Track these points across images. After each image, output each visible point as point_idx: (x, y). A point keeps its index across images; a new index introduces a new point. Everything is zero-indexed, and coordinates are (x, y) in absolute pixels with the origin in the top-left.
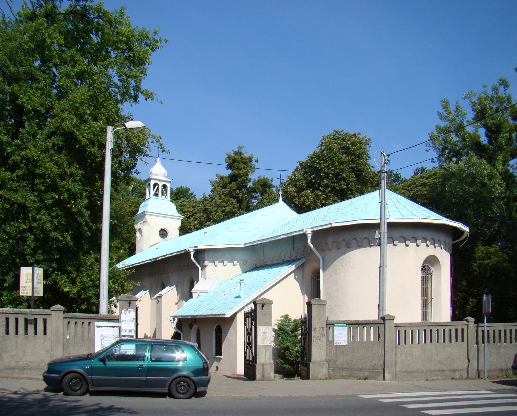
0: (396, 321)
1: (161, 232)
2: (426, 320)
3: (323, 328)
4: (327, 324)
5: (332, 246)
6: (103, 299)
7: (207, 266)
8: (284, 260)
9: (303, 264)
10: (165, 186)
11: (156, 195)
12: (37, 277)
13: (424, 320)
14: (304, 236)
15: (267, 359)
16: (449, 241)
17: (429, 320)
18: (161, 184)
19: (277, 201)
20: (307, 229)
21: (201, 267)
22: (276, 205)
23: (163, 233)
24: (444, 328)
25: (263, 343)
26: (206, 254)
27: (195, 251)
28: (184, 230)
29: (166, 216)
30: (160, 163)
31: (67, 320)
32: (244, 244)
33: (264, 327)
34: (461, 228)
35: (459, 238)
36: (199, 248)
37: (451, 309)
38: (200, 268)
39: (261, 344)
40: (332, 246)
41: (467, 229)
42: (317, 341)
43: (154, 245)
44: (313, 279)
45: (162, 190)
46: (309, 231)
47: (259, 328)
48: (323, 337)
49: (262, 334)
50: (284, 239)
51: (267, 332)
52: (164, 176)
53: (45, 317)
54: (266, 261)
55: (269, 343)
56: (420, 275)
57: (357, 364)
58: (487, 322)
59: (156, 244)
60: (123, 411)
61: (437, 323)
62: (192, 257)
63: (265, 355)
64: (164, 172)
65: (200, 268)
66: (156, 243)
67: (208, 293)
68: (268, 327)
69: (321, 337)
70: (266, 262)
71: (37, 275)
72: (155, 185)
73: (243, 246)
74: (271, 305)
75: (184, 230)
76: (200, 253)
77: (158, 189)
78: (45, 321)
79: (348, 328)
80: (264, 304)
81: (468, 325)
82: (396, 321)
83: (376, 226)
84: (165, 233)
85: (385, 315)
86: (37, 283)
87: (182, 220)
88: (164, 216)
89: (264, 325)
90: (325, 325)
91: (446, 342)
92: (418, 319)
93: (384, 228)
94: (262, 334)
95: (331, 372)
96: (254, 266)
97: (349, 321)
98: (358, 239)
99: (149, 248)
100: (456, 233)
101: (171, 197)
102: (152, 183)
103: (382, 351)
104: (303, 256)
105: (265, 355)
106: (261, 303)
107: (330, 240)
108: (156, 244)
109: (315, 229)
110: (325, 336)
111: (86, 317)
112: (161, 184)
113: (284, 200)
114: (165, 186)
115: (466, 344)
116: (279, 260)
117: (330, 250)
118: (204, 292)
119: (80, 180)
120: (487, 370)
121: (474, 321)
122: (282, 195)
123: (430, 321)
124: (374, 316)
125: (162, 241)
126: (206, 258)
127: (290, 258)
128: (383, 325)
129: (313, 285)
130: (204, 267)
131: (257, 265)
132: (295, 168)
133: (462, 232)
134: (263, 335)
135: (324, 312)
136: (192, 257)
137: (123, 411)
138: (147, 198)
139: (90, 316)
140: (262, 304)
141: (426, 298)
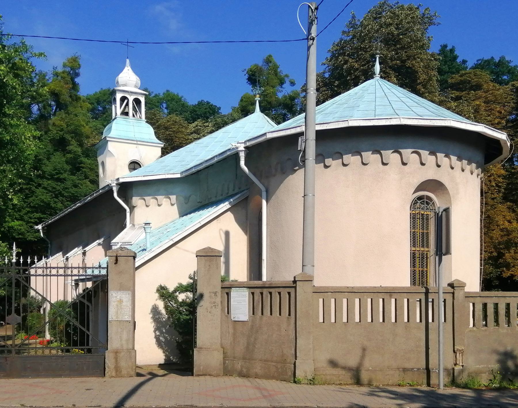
0: (467, 289)
1: (132, 165)
4: (222, 288)
7: (135, 207)
9: (247, 199)
10: (137, 102)
11: (125, 113)
14: (236, 156)
15: (124, 342)
18: (131, 98)
19: (253, 112)
20: (239, 145)
21: (130, 208)
22: (250, 117)
25: (117, 317)
29: (139, 143)
30: (129, 68)
32: (182, 173)
34: (484, 133)
37: (481, 269)
38: (128, 210)
39: (114, 318)
45: (134, 107)
46: (242, 147)
50: (218, 162)
52: (136, 86)
56: (409, 212)
60: (462, 403)
62: (115, 195)
64: (135, 80)
65: (128, 210)
67: (132, 245)
70: (211, 198)
72: (123, 99)
73: (179, 176)
77: (127, 104)
79: (249, 294)
81: (453, 293)
85: (454, 280)
87: (162, 148)
88: (136, 142)
89: (120, 290)
90: (219, 289)
91: (273, 314)
101: (146, 118)
102: (119, 96)
109: (248, 144)
112: (131, 98)
113: (263, 110)
114: (137, 102)
115: (294, 319)
116: (223, 195)
118: (127, 244)
122: (259, 101)
124: (78, 266)
126: (133, 193)
128: (293, 289)
130: (132, 208)
134: (117, 305)
135: (217, 268)
137: (462, 403)
138: (113, 118)
141: (427, 249)
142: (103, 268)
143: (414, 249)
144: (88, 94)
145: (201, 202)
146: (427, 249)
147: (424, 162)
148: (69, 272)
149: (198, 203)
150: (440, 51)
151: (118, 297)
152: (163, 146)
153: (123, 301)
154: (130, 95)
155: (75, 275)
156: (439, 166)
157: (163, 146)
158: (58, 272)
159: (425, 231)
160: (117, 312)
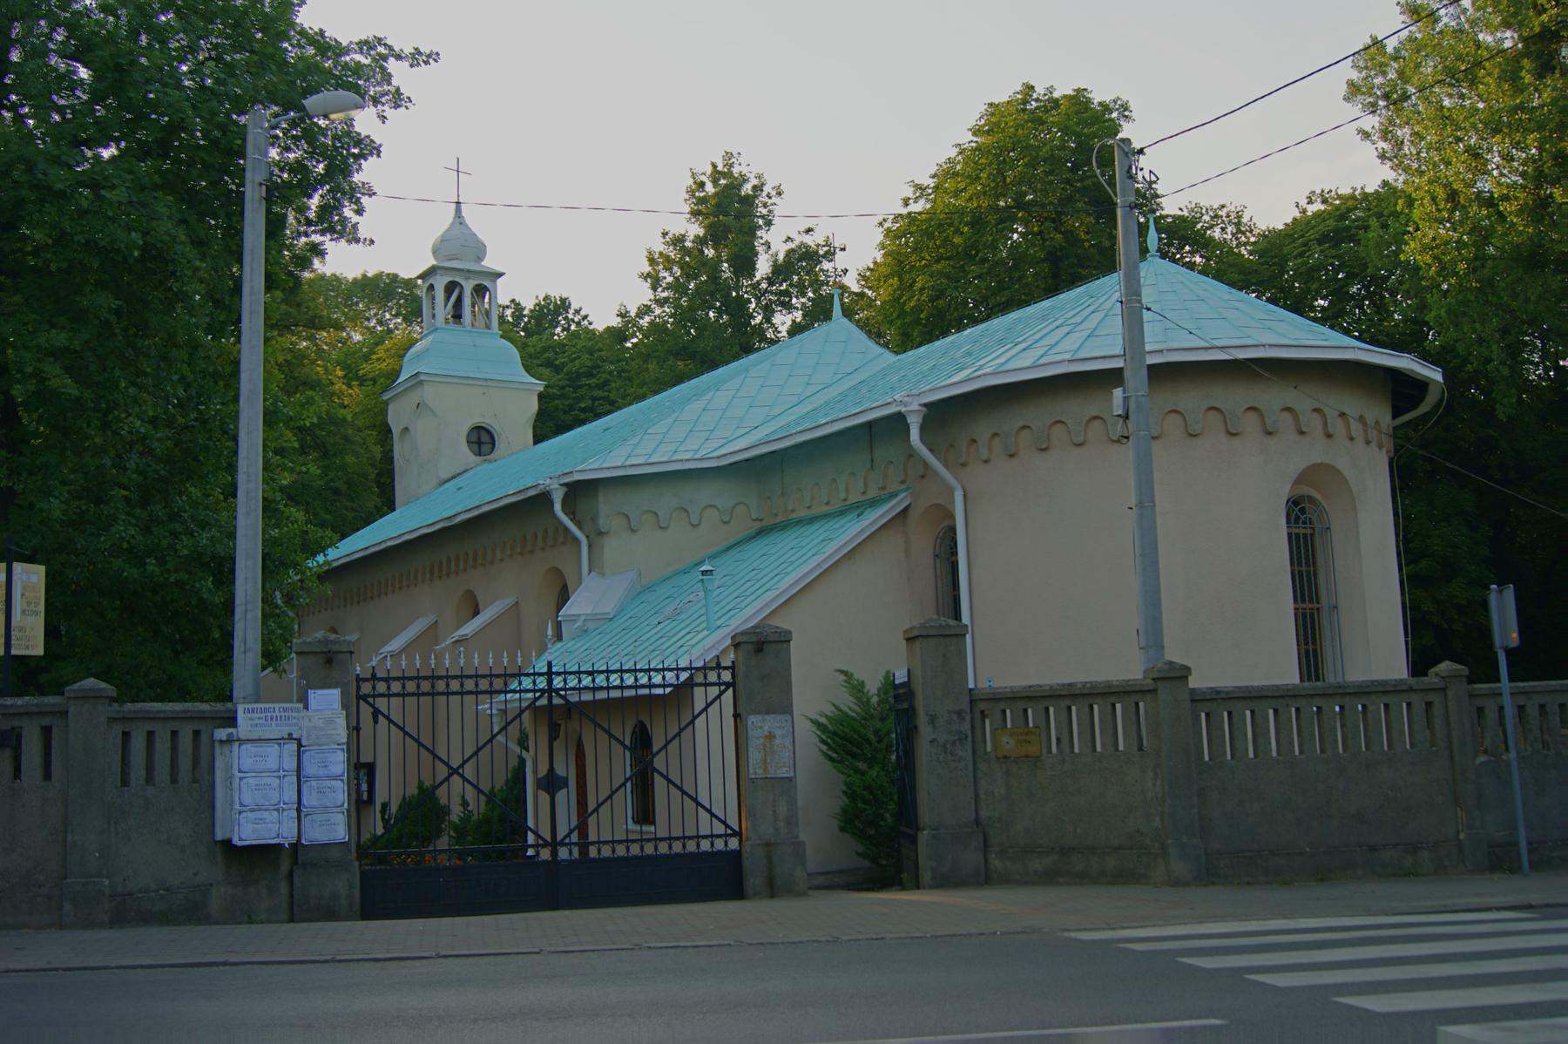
0: (1194, 682)
2: (1317, 679)
3: (959, 713)
5: (990, 449)
6: (245, 652)
8: (845, 500)
12: (23, 595)
13: (1309, 679)
14: (898, 421)
16: (1380, 413)
17: (1331, 678)
23: (482, 440)
24: (1365, 702)
25: (765, 770)
26: (601, 498)
27: (565, 489)
28: (550, 423)
31: (118, 729)
33: (768, 718)
34: (1412, 371)
35: (1415, 406)
36: (577, 477)
40: (990, 449)
41: (1435, 375)
42: (941, 758)
43: (453, 478)
44: (938, 561)
47: (749, 723)
48: (962, 744)
49: (762, 740)
51: (778, 733)
53: (46, 721)
54: (790, 508)
55: (784, 769)
57: (1079, 831)
58: (1512, 679)
59: (459, 474)
61: (1361, 685)
62: (558, 507)
63: (774, 811)
66: (458, 471)
68: (779, 717)
69: (954, 742)
70: (793, 511)
71: (24, 588)
72: (451, 287)
74: (785, 645)
75: (550, 423)
76: (580, 492)
77: (459, 300)
78: (47, 731)
80: (763, 643)
82: (1194, 682)
83: (1112, 378)
84: (485, 437)
86: (23, 612)
87: (541, 396)
90: (965, 705)
92: (1288, 673)
93: (1137, 381)
94: (762, 740)
95: (996, 862)
96: (758, 525)
97: (1041, 686)
98: (1069, 422)
99: (436, 488)
100: (1403, 389)
103: (1154, 785)
104: (903, 486)
105: (774, 811)
106: (754, 639)
107: (983, 428)
108: (459, 474)
110: (970, 739)
111: (183, 715)
117: (986, 461)
119: (1052, 155)
120: (1529, 843)
121: (1468, 677)
123: (1332, 680)
124: (1131, 669)
125: (477, 465)
127: (864, 493)
129: (939, 580)
130: (597, 536)
131: (764, 523)
132: (354, 245)
133: (1421, 385)
134: (764, 745)
136: (558, 507)
139: (199, 712)
140: (758, 643)
142: (726, 668)
143: (1301, 605)
144: (564, 304)
145: (761, 520)
146: (1315, 605)
147: (1304, 429)
148: (441, 686)
149: (754, 520)
150: (976, 132)
151: (766, 728)
152: (542, 389)
153: (775, 737)
154: (467, 279)
155: (528, 691)
156: (1329, 436)
157: (542, 389)
158: (418, 687)
159: (1304, 569)
160: (765, 759)
